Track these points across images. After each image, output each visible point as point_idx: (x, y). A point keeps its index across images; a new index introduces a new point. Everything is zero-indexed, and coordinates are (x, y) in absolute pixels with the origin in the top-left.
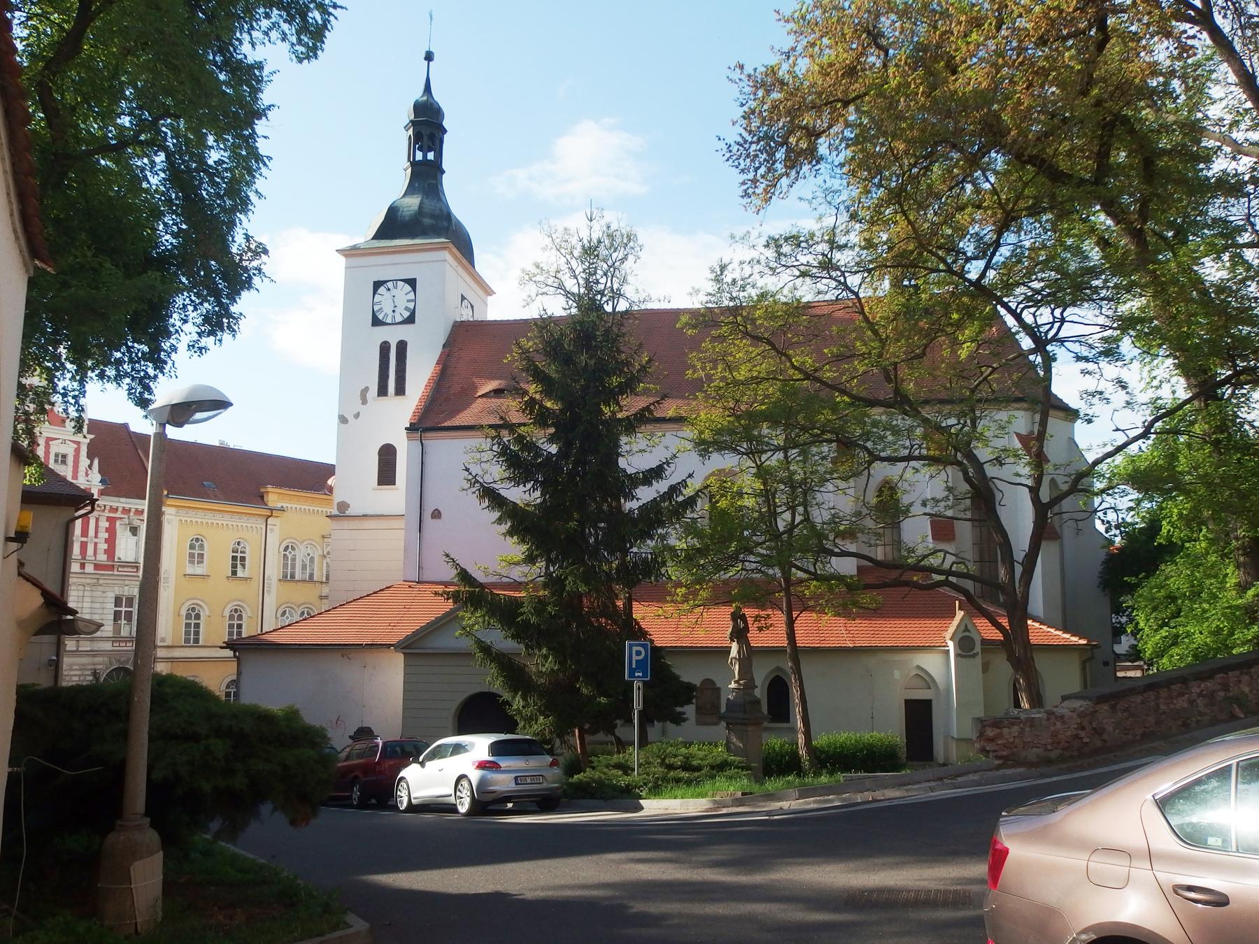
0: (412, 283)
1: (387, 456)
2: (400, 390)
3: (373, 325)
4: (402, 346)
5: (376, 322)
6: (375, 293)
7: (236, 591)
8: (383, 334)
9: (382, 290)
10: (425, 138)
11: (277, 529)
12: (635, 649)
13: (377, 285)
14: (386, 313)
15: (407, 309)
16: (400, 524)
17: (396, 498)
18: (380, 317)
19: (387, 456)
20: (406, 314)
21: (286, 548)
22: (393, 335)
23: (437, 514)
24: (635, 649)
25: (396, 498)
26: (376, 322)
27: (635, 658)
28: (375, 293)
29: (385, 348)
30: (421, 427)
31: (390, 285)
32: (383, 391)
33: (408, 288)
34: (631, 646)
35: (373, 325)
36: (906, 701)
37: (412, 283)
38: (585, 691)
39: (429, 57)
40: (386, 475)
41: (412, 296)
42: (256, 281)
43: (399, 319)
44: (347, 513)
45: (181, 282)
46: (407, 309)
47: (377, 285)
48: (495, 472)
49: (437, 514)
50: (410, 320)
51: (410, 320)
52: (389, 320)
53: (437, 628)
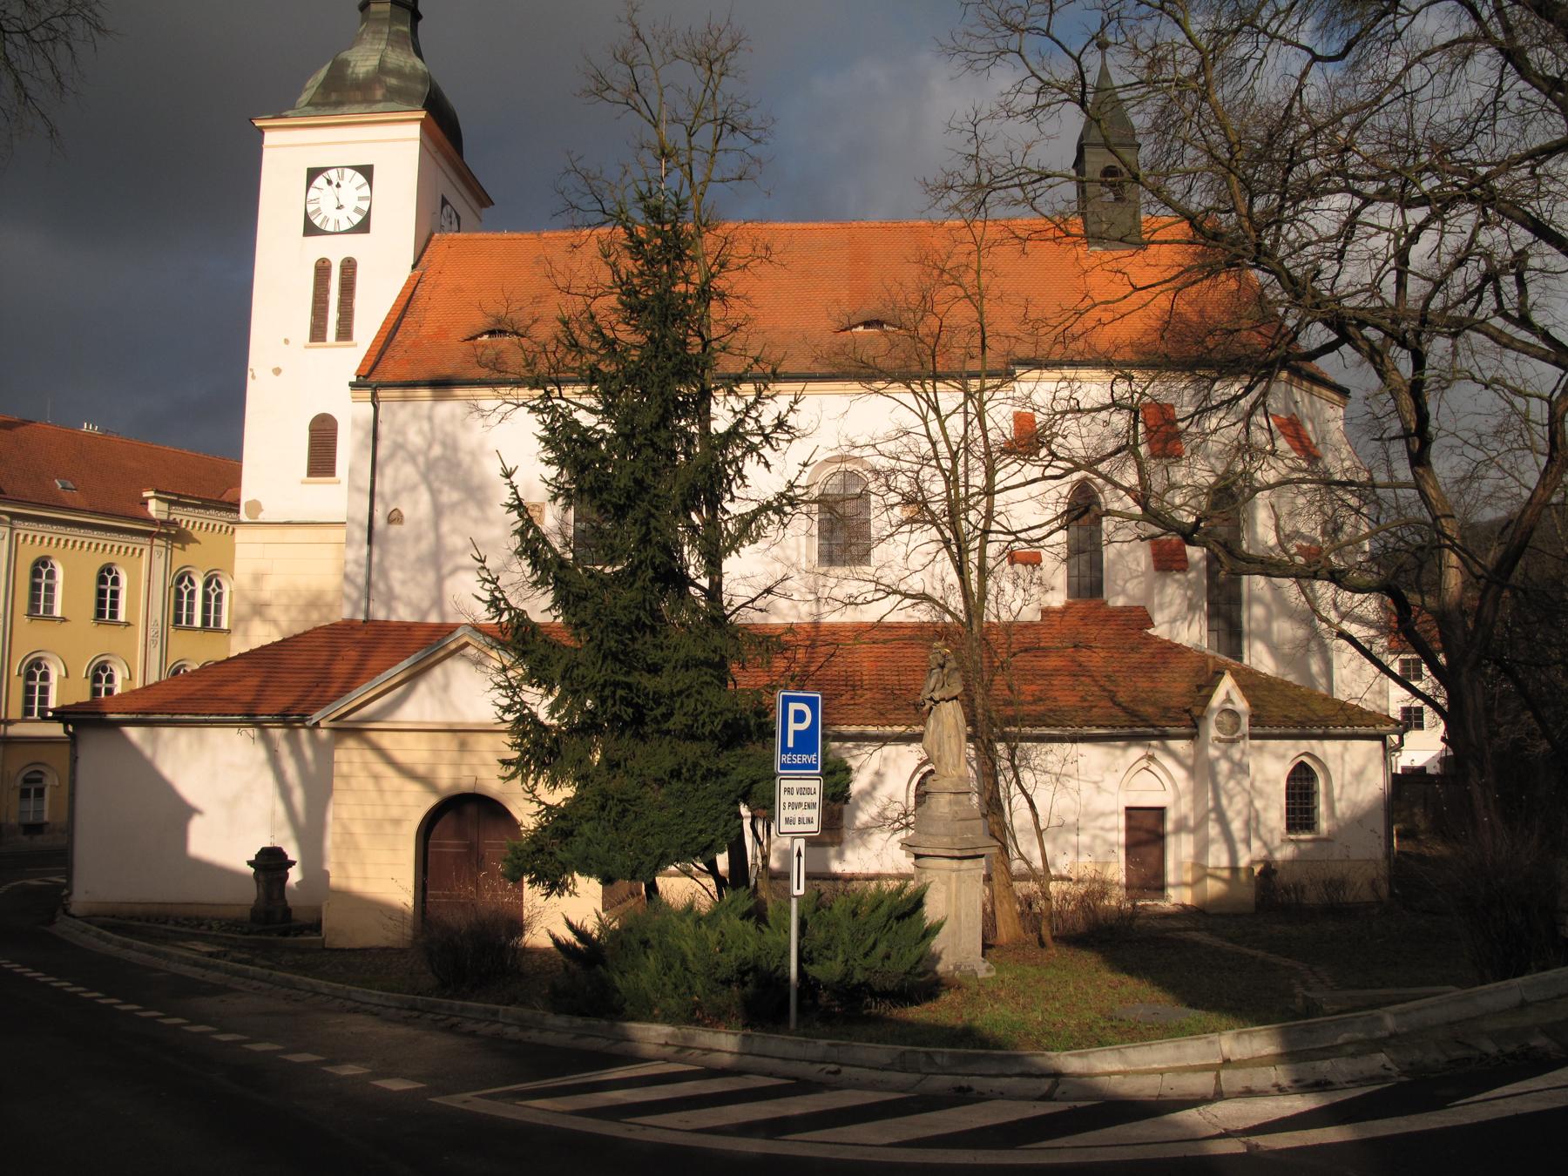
0: (367, 171)
2: (345, 333)
4: (349, 266)
5: (310, 229)
7: (101, 640)
8: (319, 247)
9: (320, 181)
12: (793, 707)
13: (313, 174)
14: (327, 216)
15: (357, 210)
16: (339, 534)
17: (336, 498)
18: (317, 222)
19: (323, 435)
20: (357, 219)
22: (335, 250)
24: (793, 707)
25: (336, 498)
26: (310, 229)
27: (793, 727)
29: (322, 269)
30: (369, 380)
31: (332, 174)
32: (318, 334)
34: (787, 700)
40: (321, 459)
43: (346, 226)
44: (262, 517)
46: (357, 210)
47: (313, 174)
48: (600, 909)
50: (363, 227)
51: (363, 227)
52: (330, 228)
53: (179, 606)
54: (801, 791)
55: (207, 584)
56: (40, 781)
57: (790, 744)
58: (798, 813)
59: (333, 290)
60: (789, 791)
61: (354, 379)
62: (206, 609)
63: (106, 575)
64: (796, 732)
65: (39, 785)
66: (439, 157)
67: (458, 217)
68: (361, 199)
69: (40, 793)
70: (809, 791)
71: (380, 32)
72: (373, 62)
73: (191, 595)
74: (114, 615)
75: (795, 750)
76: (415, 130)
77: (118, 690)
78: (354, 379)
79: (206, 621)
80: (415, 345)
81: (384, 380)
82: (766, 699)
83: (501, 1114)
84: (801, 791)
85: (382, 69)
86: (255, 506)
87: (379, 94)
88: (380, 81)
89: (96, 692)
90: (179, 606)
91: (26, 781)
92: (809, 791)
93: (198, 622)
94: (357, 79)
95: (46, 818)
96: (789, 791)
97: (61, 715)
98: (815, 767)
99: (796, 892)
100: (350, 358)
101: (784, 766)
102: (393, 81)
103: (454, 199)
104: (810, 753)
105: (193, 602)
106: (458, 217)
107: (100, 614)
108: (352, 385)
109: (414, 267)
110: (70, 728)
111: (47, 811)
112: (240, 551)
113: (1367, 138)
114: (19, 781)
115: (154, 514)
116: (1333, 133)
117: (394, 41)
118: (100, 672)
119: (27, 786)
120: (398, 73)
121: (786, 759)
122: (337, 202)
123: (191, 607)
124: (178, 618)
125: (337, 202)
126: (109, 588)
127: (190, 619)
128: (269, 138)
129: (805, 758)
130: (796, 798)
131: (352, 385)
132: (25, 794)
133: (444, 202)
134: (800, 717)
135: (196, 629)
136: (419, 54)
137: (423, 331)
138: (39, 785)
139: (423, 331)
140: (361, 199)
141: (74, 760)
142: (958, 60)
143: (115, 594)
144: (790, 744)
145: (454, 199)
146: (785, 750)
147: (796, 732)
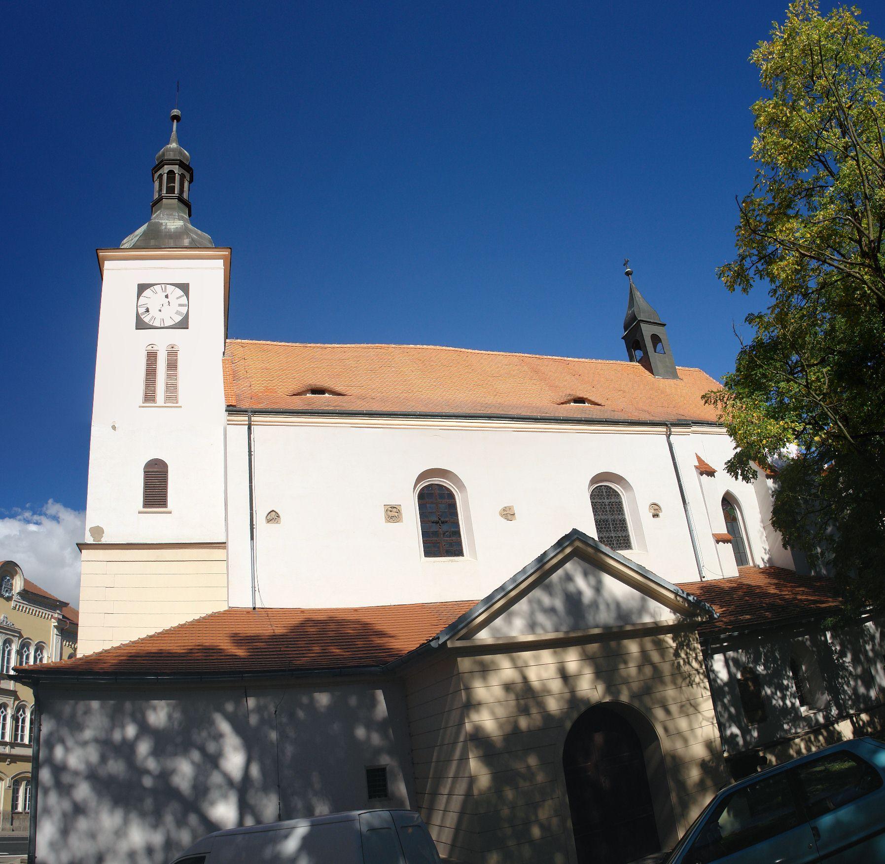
0: (185, 288)
5: (141, 325)
6: (139, 295)
10: (177, 177)
13: (142, 288)
15: (178, 313)
20: (178, 318)
22: (161, 341)
23: (273, 517)
26: (141, 325)
28: (139, 295)
29: (152, 357)
32: (149, 397)
33: (179, 292)
36: (459, 552)
37: (185, 288)
38: (826, 466)
41: (184, 300)
42: (155, 348)
43: (171, 323)
44: (105, 540)
45: (869, 605)
46: (178, 313)
47: (142, 288)
49: (273, 517)
50: (183, 324)
51: (183, 324)
68: (180, 305)
73: (23, 721)
76: (220, 263)
82: (571, 588)
83: (758, 517)
88: (188, 234)
113: (530, 775)
116: (851, 40)
123: (23, 731)
128: (107, 265)
140: (180, 305)
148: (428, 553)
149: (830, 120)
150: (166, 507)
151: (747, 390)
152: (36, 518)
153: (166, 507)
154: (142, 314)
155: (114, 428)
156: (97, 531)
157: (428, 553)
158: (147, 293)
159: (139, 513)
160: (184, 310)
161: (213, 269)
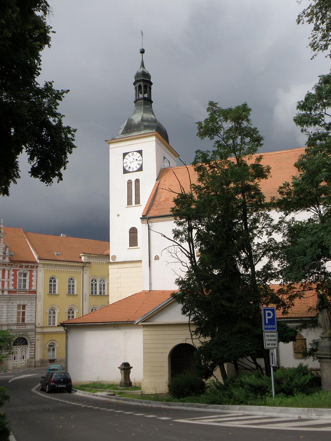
0: (140, 152)
1: (133, 232)
2: (138, 202)
3: (141, 151)
4: (137, 181)
5: (125, 172)
8: (128, 177)
11: (88, 272)
12: (267, 312)
13: (125, 155)
15: (139, 164)
18: (127, 169)
19: (133, 232)
20: (139, 167)
21: (92, 281)
22: (133, 177)
24: (267, 312)
26: (125, 172)
27: (267, 317)
29: (130, 182)
30: (146, 218)
32: (129, 203)
35: (141, 151)
37: (140, 152)
39: (142, 52)
43: (130, 154)
44: (117, 260)
46: (139, 164)
47: (125, 155)
49: (157, 258)
51: (141, 169)
52: (131, 170)
54: (271, 336)
55: (101, 281)
56: (53, 346)
57: (267, 322)
58: (271, 342)
59: (133, 192)
60: (268, 336)
61: (141, 217)
62: (100, 288)
63: (52, 280)
64: (269, 319)
65: (53, 347)
66: (162, 145)
67: (169, 162)
69: (54, 350)
70: (273, 336)
71: (141, 109)
72: (140, 118)
74: (54, 292)
75: (268, 324)
76: (154, 138)
77: (75, 317)
78: (141, 217)
79: (101, 293)
80: (159, 204)
81: (151, 216)
84: (271, 336)
85: (143, 120)
86: (114, 257)
87: (142, 128)
89: (69, 317)
90: (92, 289)
91: (50, 346)
92: (273, 336)
93: (98, 293)
94: (135, 124)
95: (55, 357)
96: (268, 336)
97: (62, 325)
98: (275, 329)
99: (272, 365)
100: (140, 210)
101: (265, 329)
102: (146, 123)
103: (167, 156)
104: (273, 325)
105: (99, 288)
106: (169, 162)
107: (50, 292)
108: (141, 218)
109: (157, 180)
110: (65, 328)
111: (58, 354)
112: (111, 271)
114: (47, 346)
115: (83, 260)
117: (145, 111)
118: (71, 311)
119: (50, 348)
120: (147, 121)
121: (266, 327)
122: (132, 162)
123: (96, 289)
124: (93, 293)
125: (132, 162)
126: (53, 283)
127: (96, 293)
129: (272, 326)
130: (270, 338)
131: (141, 218)
132: (49, 350)
133: (164, 158)
134: (269, 315)
135: (98, 295)
136: (153, 114)
137: (161, 200)
138: (53, 347)
139: (161, 200)
141: (67, 338)
142: (264, 179)
143: (55, 285)
144: (267, 322)
145: (167, 156)
146: (265, 324)
147: (269, 319)
148: (142, 170)
149: (234, 138)
150: (137, 246)
151: (292, 225)
152: (133, 120)
153: (137, 246)
154: (125, 166)
155: (118, 215)
156: (114, 257)
157: (142, 170)
158: (127, 157)
159: (128, 249)
160: (141, 163)
161: (122, 146)
